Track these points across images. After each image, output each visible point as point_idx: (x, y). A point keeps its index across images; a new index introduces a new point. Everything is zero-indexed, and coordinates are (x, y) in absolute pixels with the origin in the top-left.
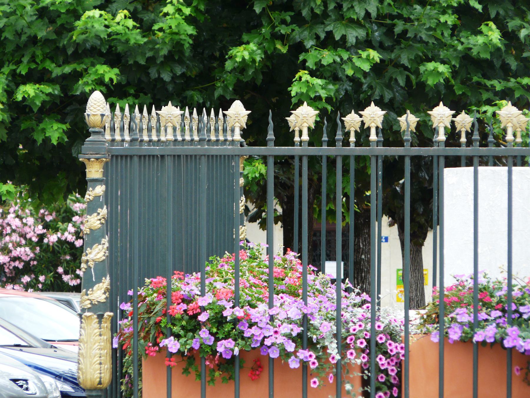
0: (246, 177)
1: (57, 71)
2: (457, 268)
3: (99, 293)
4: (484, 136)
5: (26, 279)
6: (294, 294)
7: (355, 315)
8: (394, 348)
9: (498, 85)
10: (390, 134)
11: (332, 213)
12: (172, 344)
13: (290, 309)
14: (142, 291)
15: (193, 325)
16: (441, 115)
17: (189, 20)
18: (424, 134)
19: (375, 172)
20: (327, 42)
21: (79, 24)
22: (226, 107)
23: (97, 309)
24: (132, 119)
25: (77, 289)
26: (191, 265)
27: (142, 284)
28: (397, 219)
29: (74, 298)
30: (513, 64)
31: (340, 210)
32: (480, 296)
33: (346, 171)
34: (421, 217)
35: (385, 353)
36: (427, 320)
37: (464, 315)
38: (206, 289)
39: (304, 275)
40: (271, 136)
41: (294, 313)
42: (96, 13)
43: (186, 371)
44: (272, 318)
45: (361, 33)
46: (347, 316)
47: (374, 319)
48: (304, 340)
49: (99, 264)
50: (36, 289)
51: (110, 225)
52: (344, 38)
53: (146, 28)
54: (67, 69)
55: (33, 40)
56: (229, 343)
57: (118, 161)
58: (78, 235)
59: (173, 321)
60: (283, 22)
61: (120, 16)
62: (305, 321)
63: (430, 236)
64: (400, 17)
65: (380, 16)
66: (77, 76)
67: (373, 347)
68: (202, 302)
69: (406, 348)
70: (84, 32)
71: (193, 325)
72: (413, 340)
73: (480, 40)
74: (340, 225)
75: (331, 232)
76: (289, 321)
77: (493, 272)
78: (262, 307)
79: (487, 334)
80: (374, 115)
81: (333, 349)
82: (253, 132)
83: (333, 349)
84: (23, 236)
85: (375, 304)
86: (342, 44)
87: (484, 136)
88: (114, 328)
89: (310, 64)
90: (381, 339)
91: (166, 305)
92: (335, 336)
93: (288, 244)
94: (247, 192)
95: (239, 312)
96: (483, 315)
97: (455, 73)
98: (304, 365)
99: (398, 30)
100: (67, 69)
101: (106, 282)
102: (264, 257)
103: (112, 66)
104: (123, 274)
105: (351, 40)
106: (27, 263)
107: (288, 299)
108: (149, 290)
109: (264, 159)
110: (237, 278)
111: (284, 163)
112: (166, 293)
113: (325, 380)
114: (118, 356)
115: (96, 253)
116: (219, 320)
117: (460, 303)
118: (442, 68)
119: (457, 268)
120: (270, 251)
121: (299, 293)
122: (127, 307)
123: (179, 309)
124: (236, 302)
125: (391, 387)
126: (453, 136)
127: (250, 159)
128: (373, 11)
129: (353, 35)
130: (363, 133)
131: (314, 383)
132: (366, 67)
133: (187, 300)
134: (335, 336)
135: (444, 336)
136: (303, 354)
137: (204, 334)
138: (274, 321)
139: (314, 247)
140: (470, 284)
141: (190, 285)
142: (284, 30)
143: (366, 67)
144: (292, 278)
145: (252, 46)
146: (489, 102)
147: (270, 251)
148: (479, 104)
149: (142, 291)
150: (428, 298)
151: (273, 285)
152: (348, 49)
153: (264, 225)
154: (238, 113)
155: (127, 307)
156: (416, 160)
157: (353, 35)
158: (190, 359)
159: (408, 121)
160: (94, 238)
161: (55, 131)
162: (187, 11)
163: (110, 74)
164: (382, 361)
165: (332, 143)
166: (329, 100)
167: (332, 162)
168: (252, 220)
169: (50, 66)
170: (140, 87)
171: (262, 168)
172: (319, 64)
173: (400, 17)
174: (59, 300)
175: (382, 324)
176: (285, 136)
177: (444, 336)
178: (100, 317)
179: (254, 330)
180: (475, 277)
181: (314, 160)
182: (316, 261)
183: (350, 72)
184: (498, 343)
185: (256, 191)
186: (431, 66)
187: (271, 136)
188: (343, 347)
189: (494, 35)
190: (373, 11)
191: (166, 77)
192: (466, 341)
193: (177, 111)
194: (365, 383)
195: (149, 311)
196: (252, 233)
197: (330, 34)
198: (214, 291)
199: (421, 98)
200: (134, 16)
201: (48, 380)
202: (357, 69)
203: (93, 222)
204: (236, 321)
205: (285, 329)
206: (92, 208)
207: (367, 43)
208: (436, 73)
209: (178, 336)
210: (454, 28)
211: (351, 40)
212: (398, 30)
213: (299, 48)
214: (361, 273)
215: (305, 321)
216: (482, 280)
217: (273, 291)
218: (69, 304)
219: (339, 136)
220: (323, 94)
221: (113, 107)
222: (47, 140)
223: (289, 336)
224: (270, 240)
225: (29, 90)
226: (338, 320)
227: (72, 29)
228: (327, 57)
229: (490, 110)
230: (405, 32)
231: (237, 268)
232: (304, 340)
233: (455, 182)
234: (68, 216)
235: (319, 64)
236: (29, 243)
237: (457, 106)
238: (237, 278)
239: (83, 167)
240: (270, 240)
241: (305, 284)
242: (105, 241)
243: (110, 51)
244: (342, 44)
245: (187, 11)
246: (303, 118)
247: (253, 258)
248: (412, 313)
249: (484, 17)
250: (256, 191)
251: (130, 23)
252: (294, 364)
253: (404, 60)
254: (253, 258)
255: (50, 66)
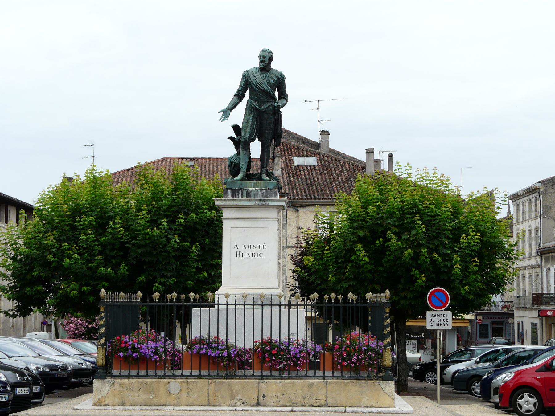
0: (142, 311)
1: (92, 283)
2: (196, 334)
3: (102, 341)
4: (203, 300)
5: (83, 337)
6: (153, 341)
7: (169, 346)
8: (179, 355)
9: (206, 287)
10: (178, 299)
11: (163, 320)
12: (121, 354)
13: (152, 345)
14: (114, 340)
15: (127, 349)
16: (192, 294)
17: (127, 270)
18: (188, 299)
19: (175, 310)
20: (162, 276)
21: (98, 271)
22: (136, 293)
23: (102, 345)
24: (112, 296)
25: (96, 339)
26: (127, 333)
27: (114, 338)
28: (180, 321)
29: (96, 342)
30: (210, 282)
31: (165, 319)
32: (201, 341)
33: (167, 309)
34: (187, 320)
35: (177, 356)
36: (187, 348)
37: (197, 347)
38: (129, 340)
39: (156, 336)
40: (148, 300)
41: (153, 346)
42: (103, 268)
43: (125, 361)
44: (148, 347)
45: (171, 274)
46: (167, 346)
47: (174, 347)
48: (156, 353)
49: (102, 333)
50: (85, 339)
51: (106, 324)
52: (167, 275)
53: (116, 272)
54: (95, 283)
55: (86, 275)
56: (136, 354)
57: (108, 307)
58: (97, 325)
59: (122, 348)
60: (151, 271)
61: (109, 269)
62: (156, 348)
63: (188, 326)
64: (181, 270)
65: (176, 269)
66: (98, 284)
67: (174, 355)
68: (129, 343)
69: (182, 355)
70: (100, 273)
71: (127, 349)
72: (184, 353)
73: (202, 275)
74: (165, 323)
75: (163, 324)
76: (152, 348)
77: (205, 335)
78: (145, 344)
79: (204, 351)
80: (175, 294)
81: (163, 355)
82: (143, 299)
83: (163, 355)
84: (82, 325)
85: (174, 343)
86: (167, 276)
87: (203, 300)
88: (106, 350)
89: (158, 282)
90: (176, 353)
91: (120, 344)
92: (164, 352)
93: (152, 328)
94: (141, 314)
95: (139, 346)
96: (202, 347)
97: (195, 284)
98: (156, 359)
99: (181, 273)
100: (95, 283)
101: (104, 338)
102: (146, 331)
103: (107, 282)
104: (109, 335)
105: (169, 275)
106: (83, 333)
107: (152, 342)
108: (116, 340)
109: (146, 306)
110: (139, 337)
111: (151, 307)
112: (120, 341)
113: (161, 363)
114: (107, 358)
115: (102, 331)
116: (133, 348)
117: (196, 343)
118: (192, 283)
119: (196, 334)
120: (147, 330)
121: (155, 340)
122: (110, 345)
123: (124, 345)
124: (138, 343)
125: (178, 365)
126: (195, 299)
127: (143, 306)
128: (174, 268)
129: (169, 274)
130: (172, 299)
131: (158, 364)
132: (172, 282)
133: (126, 343)
134: (164, 352)
135: (192, 352)
136: (155, 357)
137: (130, 351)
138: (149, 347)
139: (159, 328)
140: (199, 338)
141: (126, 339)
142: (151, 273)
143: (172, 282)
144: (153, 337)
145: (143, 277)
146: (204, 292)
147: (147, 330)
148: (202, 292)
149: (114, 340)
150: (188, 342)
151: (148, 338)
152: (168, 278)
153: (145, 323)
154: (139, 294)
155: (110, 345)
156: (185, 306)
157: (169, 274)
158: (126, 358)
159: (183, 296)
160: (102, 326)
161: (92, 299)
162: (126, 268)
163: (106, 284)
164: (176, 358)
165: (163, 302)
166: (163, 291)
167: (163, 307)
168: (142, 322)
169: (91, 282)
170: (113, 288)
171: (146, 308)
172: (160, 282)
173: (181, 270)
174: (22, 342)
175: (176, 349)
176: (152, 300)
177: (192, 352)
178: (103, 347)
179: (143, 351)
180: (262, 339)
181: (159, 306)
182: (158, 332)
183: (168, 284)
184: (206, 353)
185: (144, 314)
186: (189, 282)
187: (148, 300)
188: (166, 355)
189: (205, 274)
190: (174, 268)
191: (121, 285)
192: (198, 353)
193: (124, 294)
194: (171, 364)
195: (115, 345)
196: (143, 325)
197: (163, 274)
198: (132, 340)
199: (187, 291)
200: (112, 269)
201: (88, 363)
202: (170, 283)
203: (102, 322)
204: (138, 348)
205: (151, 350)
206: (101, 319)
207: (172, 276)
208: (190, 284)
209: (123, 352)
210: (195, 272)
211: (169, 275)
212: (181, 273)
213: (155, 277)
214: (171, 336)
215: (156, 348)
216: (202, 337)
217: (148, 340)
218: (94, 343)
219: (166, 300)
220: (161, 289)
221: (107, 293)
222: (89, 301)
223: (152, 352)
224: (147, 327)
225: (85, 288)
226: (165, 348)
227: (96, 272)
228: (163, 280)
229: (204, 294)
230: (182, 274)
231: (139, 334)
232: (156, 353)
233: (195, 312)
234: (94, 320)
235: (160, 282)
236: (84, 327)
237: (196, 293)
238: (139, 337)
239: (99, 308)
240: (147, 327)
241: (156, 339)
242: (104, 327)
243: (106, 278)
244: (167, 276)
245: (126, 268)
246: (157, 295)
247: (143, 331)
248: (184, 346)
249: (203, 270)
250: (144, 314)
251: (112, 271)
252: (153, 359)
253: (182, 281)
254: (143, 331)
255: (91, 282)
